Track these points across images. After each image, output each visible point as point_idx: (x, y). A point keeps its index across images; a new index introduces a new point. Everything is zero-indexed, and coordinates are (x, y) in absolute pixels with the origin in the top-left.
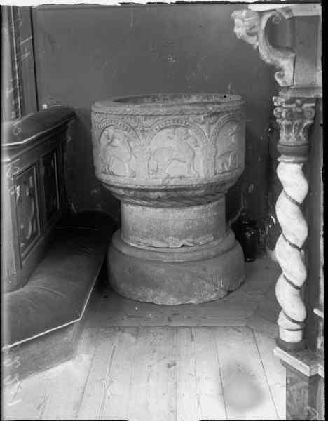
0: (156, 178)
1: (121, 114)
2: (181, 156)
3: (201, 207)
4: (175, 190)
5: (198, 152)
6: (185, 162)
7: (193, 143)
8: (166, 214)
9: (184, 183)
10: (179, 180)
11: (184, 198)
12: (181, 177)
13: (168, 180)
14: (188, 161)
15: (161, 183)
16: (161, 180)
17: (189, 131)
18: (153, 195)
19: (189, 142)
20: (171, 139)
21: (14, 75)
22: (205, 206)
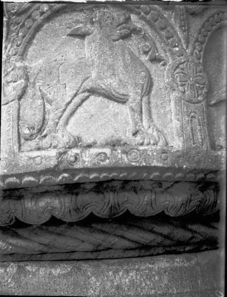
0: (39, 149)
1: (182, 117)
2: (110, 83)
3: (178, 261)
4: (100, 187)
5: (162, 76)
6: (124, 102)
7: (129, 27)
8: (81, 279)
9: (126, 160)
10: (107, 151)
11: (128, 220)
12: (114, 144)
13: (75, 151)
14: (133, 94)
15: (53, 163)
16: (53, 153)
17: (133, 17)
18: (36, 209)
19: (134, 49)
20: (83, 36)
21: (118, 98)
22: (189, 260)
